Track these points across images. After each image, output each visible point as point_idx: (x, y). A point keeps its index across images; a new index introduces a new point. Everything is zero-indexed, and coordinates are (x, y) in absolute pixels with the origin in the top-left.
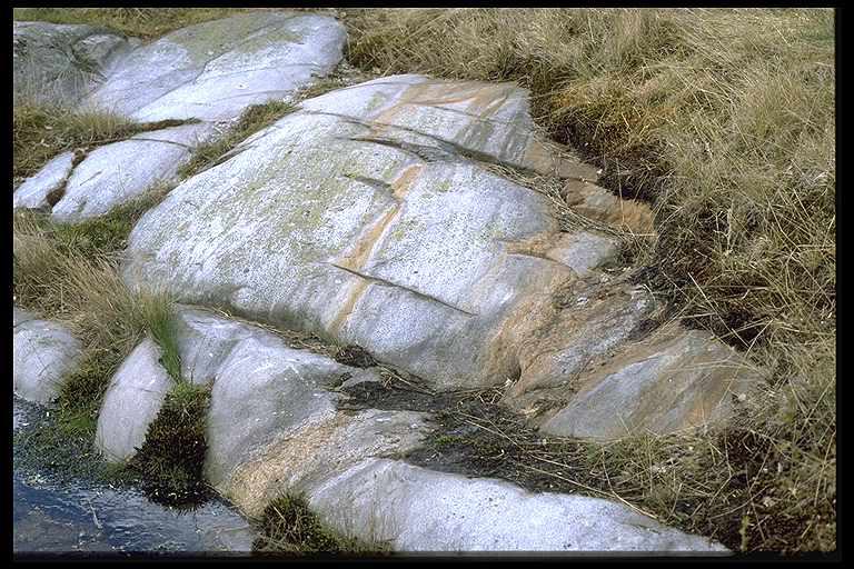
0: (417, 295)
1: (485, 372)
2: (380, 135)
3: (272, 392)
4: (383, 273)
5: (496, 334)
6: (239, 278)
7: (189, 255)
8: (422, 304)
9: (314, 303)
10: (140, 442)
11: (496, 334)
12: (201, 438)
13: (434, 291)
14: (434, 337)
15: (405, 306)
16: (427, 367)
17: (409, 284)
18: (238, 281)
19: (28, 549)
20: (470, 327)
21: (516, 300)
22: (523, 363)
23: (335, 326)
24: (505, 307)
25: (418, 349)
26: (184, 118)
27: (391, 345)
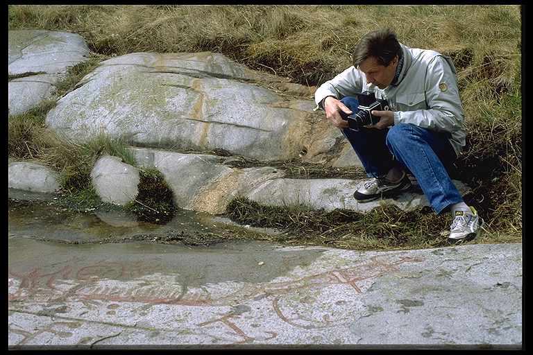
0: (237, 126)
1: (288, 153)
2: (163, 70)
3: (479, 115)
4: (214, 119)
5: (286, 137)
6: (134, 130)
7: (94, 125)
8: (243, 129)
9: (184, 135)
10: (137, 192)
11: (286, 137)
12: (167, 187)
13: (245, 123)
14: (255, 141)
15: (235, 130)
16: (258, 154)
17: (232, 121)
18: (133, 131)
19: (15, 347)
20: (272, 136)
21: (288, 124)
22: (307, 146)
23: (202, 142)
24: (284, 127)
25: (251, 146)
26: (35, 72)
27: (236, 147)
